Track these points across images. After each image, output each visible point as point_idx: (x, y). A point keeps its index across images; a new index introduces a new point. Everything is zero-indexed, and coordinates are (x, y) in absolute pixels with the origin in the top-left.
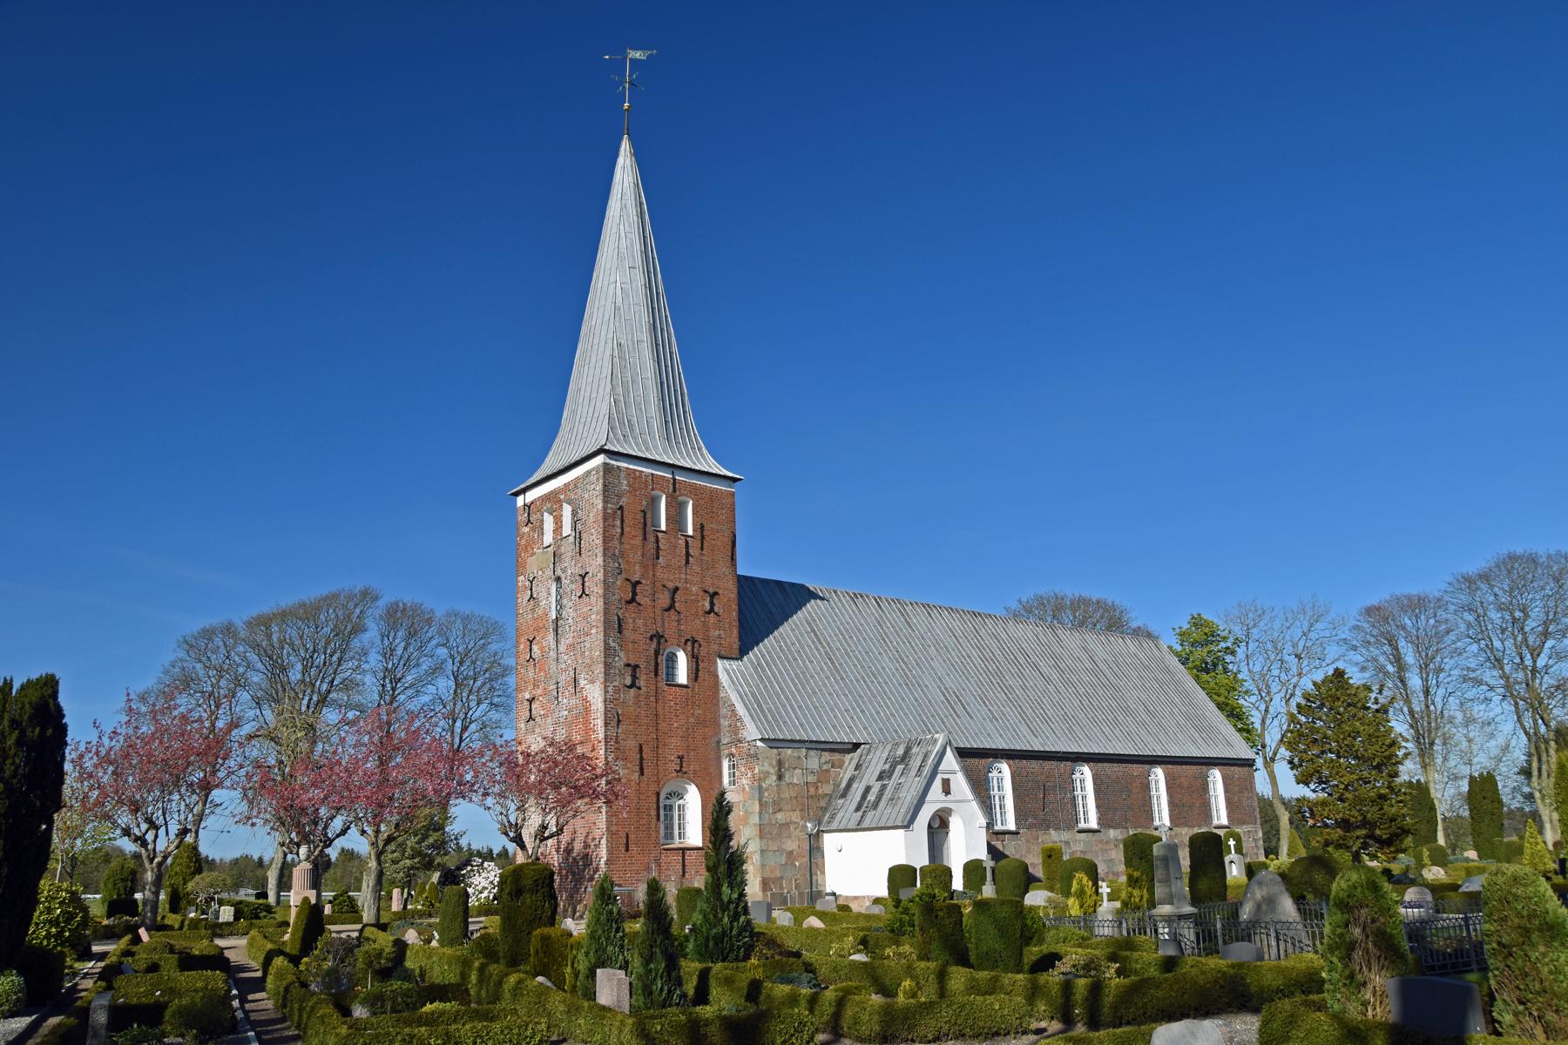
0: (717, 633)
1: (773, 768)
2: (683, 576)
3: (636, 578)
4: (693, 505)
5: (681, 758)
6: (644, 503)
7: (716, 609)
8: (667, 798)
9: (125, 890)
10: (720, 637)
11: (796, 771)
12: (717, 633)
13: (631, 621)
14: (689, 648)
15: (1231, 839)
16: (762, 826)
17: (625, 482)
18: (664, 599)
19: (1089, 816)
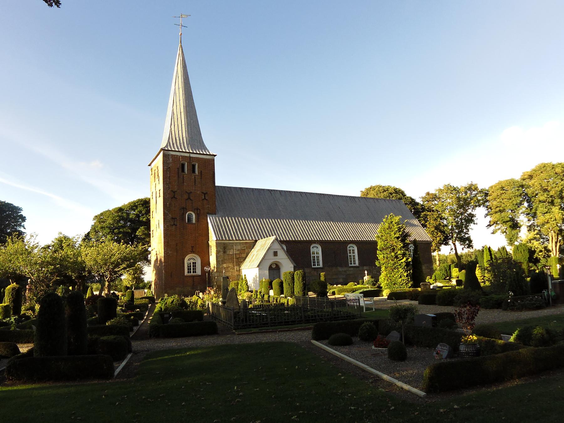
0: (207, 206)
1: (222, 249)
2: (194, 188)
3: (176, 190)
4: (198, 165)
5: (192, 247)
6: (178, 165)
7: (205, 200)
8: (313, 248)
9: (261, 297)
10: (208, 207)
11: (231, 250)
12: (207, 206)
13: (173, 204)
14: (196, 212)
15: (366, 271)
16: (217, 268)
17: (171, 159)
18: (186, 196)
19: (320, 264)
